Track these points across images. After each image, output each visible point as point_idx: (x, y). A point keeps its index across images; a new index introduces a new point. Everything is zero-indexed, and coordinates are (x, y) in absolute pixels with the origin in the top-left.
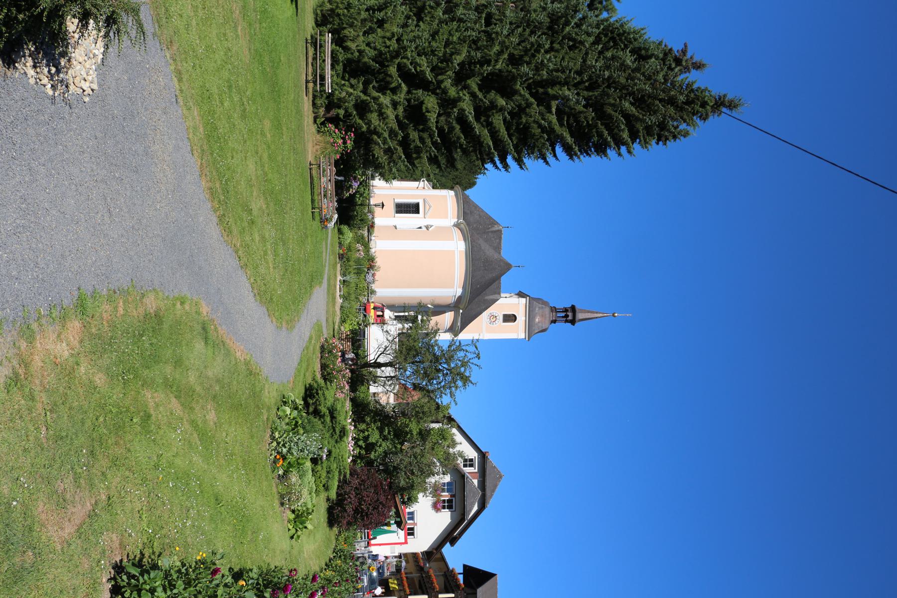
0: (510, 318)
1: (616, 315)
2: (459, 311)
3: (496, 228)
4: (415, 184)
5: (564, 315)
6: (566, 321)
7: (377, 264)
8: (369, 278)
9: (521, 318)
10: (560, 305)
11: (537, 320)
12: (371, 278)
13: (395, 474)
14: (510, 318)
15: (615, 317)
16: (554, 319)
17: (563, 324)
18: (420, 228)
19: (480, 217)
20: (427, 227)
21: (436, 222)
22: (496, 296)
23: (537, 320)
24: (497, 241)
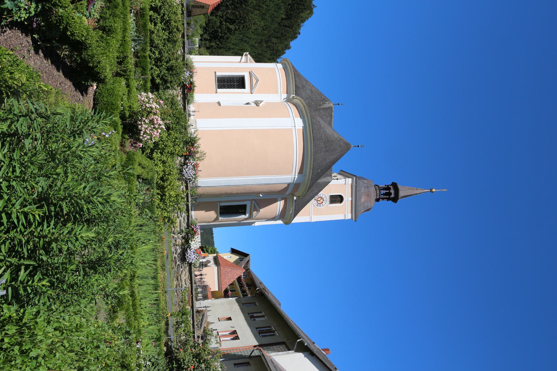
0: (337, 199)
1: (434, 190)
2: (293, 198)
3: (327, 105)
4: (239, 58)
6: (388, 199)
7: (199, 150)
9: (348, 199)
11: (363, 200)
12: (192, 172)
14: (337, 199)
15: (433, 192)
16: (378, 197)
18: (248, 104)
19: (312, 92)
20: (257, 103)
21: (266, 98)
22: (328, 178)
23: (363, 200)
24: (329, 119)
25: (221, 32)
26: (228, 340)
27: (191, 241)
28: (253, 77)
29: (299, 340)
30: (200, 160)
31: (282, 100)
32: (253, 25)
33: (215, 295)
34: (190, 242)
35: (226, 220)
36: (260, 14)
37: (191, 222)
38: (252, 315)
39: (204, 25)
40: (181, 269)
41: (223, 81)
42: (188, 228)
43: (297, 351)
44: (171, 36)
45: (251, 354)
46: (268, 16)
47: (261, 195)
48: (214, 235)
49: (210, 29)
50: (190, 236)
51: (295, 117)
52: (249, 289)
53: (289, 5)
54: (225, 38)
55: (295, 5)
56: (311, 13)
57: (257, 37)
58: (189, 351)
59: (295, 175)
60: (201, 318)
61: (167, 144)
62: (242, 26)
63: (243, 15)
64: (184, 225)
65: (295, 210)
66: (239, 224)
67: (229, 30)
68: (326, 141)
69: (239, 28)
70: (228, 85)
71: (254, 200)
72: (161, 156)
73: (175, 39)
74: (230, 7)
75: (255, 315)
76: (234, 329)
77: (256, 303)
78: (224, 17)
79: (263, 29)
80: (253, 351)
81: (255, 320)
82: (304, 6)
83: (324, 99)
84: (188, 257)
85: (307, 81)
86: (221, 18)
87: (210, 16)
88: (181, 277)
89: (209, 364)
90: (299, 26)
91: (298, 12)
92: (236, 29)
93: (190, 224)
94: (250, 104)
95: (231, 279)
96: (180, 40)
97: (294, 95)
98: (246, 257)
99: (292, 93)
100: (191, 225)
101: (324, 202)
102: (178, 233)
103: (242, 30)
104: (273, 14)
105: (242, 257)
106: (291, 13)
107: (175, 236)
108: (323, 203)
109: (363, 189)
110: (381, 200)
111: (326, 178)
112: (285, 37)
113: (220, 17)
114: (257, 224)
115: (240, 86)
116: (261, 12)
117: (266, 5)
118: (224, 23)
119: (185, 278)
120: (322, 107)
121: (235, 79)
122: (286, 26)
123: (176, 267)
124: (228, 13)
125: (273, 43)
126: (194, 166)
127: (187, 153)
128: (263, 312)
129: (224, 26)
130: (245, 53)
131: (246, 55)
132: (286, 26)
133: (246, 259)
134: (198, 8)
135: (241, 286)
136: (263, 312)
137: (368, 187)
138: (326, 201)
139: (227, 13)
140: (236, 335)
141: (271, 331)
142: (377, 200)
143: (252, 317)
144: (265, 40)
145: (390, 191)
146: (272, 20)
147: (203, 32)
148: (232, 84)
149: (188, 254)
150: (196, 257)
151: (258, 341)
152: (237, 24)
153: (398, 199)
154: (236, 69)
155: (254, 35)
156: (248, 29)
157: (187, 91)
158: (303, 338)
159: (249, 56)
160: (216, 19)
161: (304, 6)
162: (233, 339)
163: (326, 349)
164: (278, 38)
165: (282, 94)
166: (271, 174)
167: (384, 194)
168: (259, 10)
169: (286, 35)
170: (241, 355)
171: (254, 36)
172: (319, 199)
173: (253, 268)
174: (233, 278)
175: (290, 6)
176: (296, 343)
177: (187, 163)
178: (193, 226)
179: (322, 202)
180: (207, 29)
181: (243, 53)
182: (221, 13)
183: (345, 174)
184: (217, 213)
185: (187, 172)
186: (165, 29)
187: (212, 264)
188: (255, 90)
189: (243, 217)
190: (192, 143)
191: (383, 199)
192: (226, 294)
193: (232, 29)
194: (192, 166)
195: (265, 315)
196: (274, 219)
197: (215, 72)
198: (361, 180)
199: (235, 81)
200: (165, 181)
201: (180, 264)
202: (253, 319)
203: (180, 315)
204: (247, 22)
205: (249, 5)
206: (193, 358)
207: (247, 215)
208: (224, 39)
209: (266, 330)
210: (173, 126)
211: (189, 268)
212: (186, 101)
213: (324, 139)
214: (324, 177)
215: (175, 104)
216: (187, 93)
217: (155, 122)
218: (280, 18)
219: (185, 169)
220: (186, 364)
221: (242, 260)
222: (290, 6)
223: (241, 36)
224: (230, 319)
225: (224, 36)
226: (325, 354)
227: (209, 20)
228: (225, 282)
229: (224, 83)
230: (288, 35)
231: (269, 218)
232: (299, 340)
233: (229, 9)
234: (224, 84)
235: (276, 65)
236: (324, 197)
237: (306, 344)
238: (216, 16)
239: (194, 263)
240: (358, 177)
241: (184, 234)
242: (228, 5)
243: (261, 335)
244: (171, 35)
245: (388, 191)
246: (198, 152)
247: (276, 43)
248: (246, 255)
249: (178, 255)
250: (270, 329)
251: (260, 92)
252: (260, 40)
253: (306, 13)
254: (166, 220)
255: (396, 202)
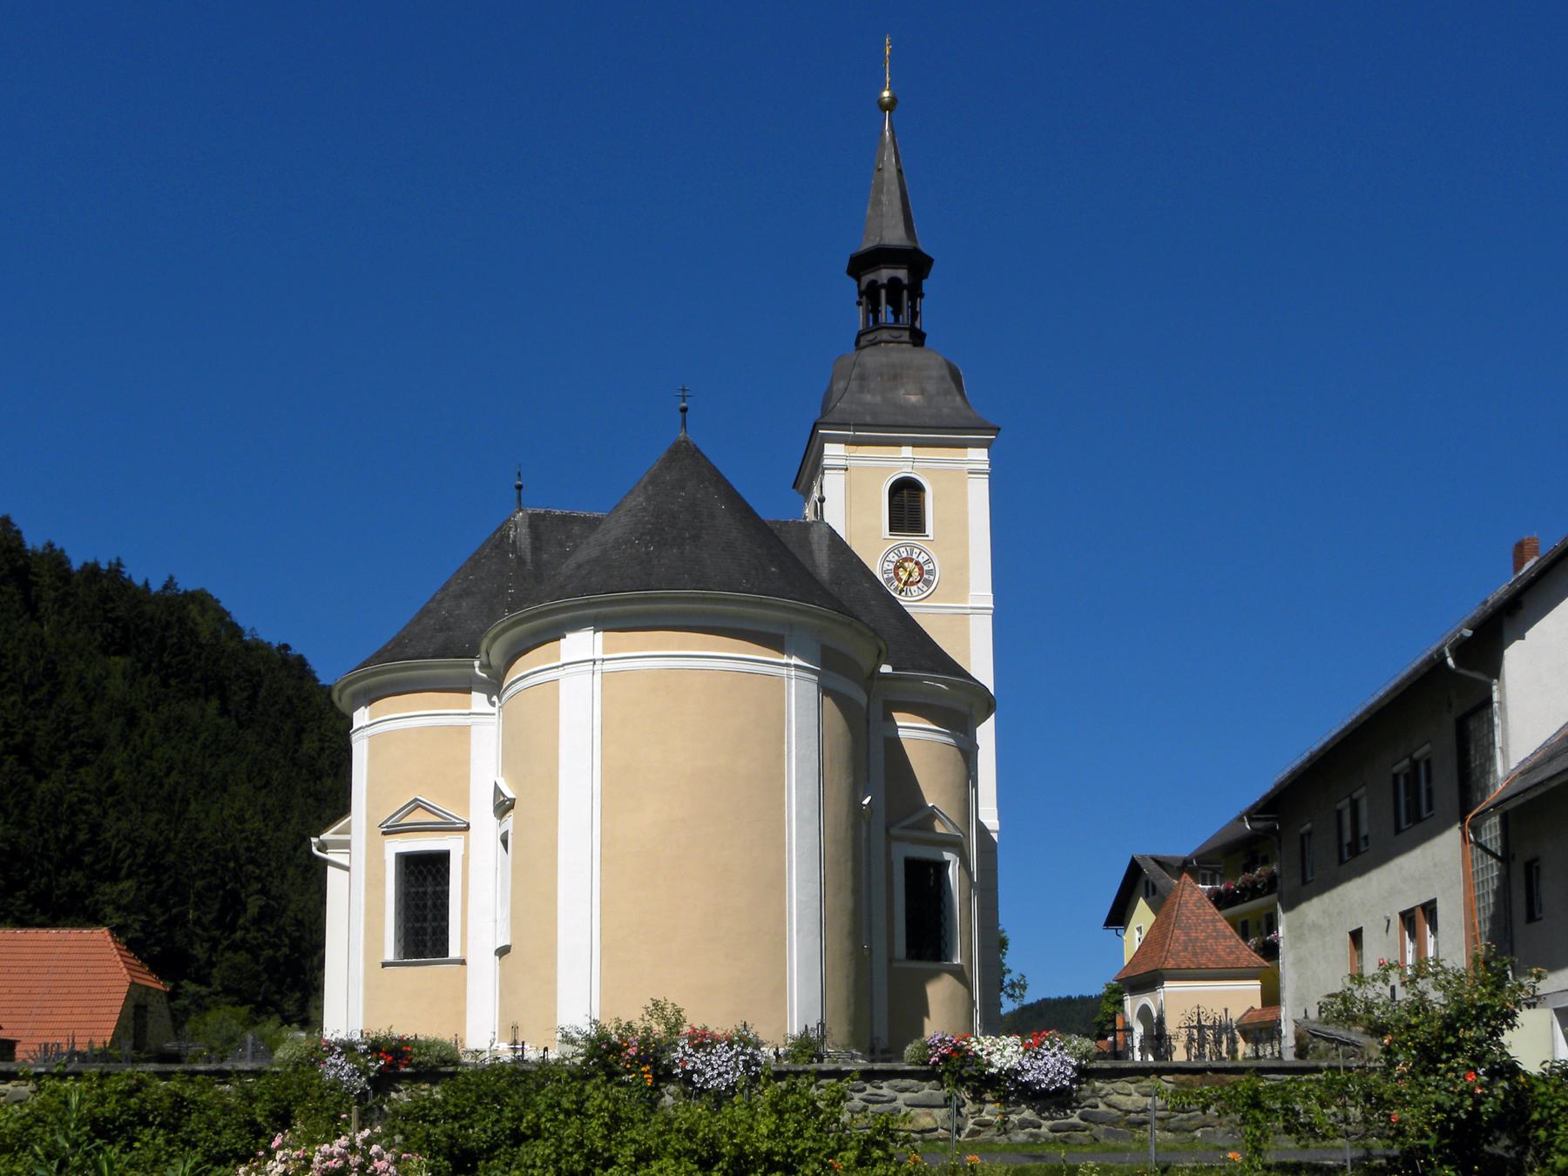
1: (886, 94)
3: (520, 533)
5: (890, 309)
6: (916, 292)
7: (638, 1025)
8: (718, 1069)
9: (905, 461)
10: (858, 317)
12: (721, 1055)
13: (567, 1062)
16: (906, 336)
17: (924, 305)
18: (505, 842)
20: (503, 807)
23: (913, 399)
25: (276, 947)
26: (1436, 944)
27: (990, 1064)
28: (404, 821)
29: (1450, 661)
30: (679, 1023)
31: (494, 710)
32: (247, 826)
33: (1271, 997)
34: (993, 1070)
35: (965, 939)
36: (205, 797)
37: (916, 1064)
38: (1346, 850)
39: (244, 1010)
40: (1102, 1108)
41: (417, 934)
42: (939, 1077)
43: (1495, 669)
44: (159, 1119)
45: (1494, 855)
46: (213, 766)
47: (866, 802)
48: (1075, 994)
49: (260, 986)
50: (969, 1069)
51: (559, 659)
52: (1265, 861)
53: (165, 683)
54: (297, 934)
55: (166, 660)
56: (201, 599)
57: (297, 813)
58: (1403, 1086)
59: (787, 665)
60: (1322, 1045)
61: (571, 1141)
62: (250, 868)
63: (207, 862)
64: (926, 1091)
65: (932, 671)
66: (986, 888)
67: (263, 917)
68: (657, 538)
69: (258, 879)
70: (435, 919)
71: (887, 830)
72: (620, 1166)
73: (167, 1102)
74: (174, 911)
75: (1347, 837)
76: (1396, 921)
77: (1302, 830)
78: (217, 933)
79: (267, 784)
80: (1480, 846)
81: (1366, 838)
82: (168, 623)
83: (497, 547)
84: (1052, 1081)
85: (425, 612)
86: (221, 947)
87: (209, 985)
88: (1130, 1112)
89: (1466, 1010)
90: (256, 648)
91: (194, 650)
92: (263, 892)
93: (924, 1068)
94: (507, 832)
95: (1215, 930)
96: (173, 1085)
97: (477, 663)
98: (1141, 870)
99: (469, 670)
100: (926, 1063)
101: (914, 556)
102: (959, 1113)
103: (267, 869)
104: (205, 747)
105: (1141, 887)
106: (198, 675)
107: (970, 1125)
108: (921, 561)
109: (868, 398)
110: (918, 325)
111: (815, 547)
112: (295, 701)
113: (213, 949)
114: (989, 815)
115: (438, 871)
116: (196, 793)
117: (168, 774)
118: (239, 934)
119: (1136, 1096)
120: (528, 556)
121: (413, 890)
122: (252, 698)
123: (1092, 1125)
124: (199, 918)
125: (322, 749)
126: (696, 1048)
127: (648, 1073)
128: (1339, 806)
129: (249, 936)
130: (314, 850)
131: (323, 847)
132: (252, 698)
133: (1149, 869)
134: (145, 1026)
135: (1251, 892)
136: (1339, 806)
137: (862, 378)
138: (913, 547)
139: (198, 922)
140: (1419, 913)
141: (1412, 777)
142: (918, 338)
143: (1355, 849)
144: (307, 781)
145: (883, 286)
146: (230, 750)
147: (272, 1014)
148: (430, 903)
149: (1040, 1082)
150: (1055, 1049)
151: (1447, 826)
152: (243, 886)
153: (916, 251)
154: (374, 884)
155: (288, 821)
156: (264, 844)
157: (406, 1066)
158: (1443, 646)
159: (326, 836)
160: (225, 965)
161: (168, 623)
162: (1434, 929)
163: (1515, 556)
164: (302, 730)
165: (473, 710)
166: (780, 756)
167: (897, 313)
168: (185, 802)
169: (289, 700)
170: (1496, 893)
171: (294, 821)
172: (904, 577)
173: (1184, 847)
174: (1214, 921)
175: (173, 682)
176: (1462, 671)
177: (685, 1072)
178: (931, 1056)
179: (917, 563)
180: (260, 998)
181: (317, 858)
182: (197, 946)
183: (809, 470)
184: (935, 975)
185: (720, 1075)
186: (128, 1138)
187: (1154, 1001)
188: (455, 812)
189: (953, 873)
190: (608, 1052)
191: (914, 315)
192: (1270, 951)
193: (261, 907)
194: (697, 1052)
195: (1350, 795)
196: (968, 754)
197: (384, 965)
198: (832, 404)
199: (421, 890)
200: (714, 1152)
201: (1079, 1111)
202: (1362, 843)
203: (1260, 1116)
204: (234, 846)
205: (167, 839)
206: (1436, 1071)
207: (948, 856)
208: (301, 938)
209: (1407, 794)
210: (508, 1119)
211: (1097, 1079)
212: (442, 1069)
213: (647, 547)
214: (811, 552)
215: (424, 1108)
216: (413, 1066)
217: (337, 1166)
218: (221, 721)
219: (706, 1081)
220: (1457, 1099)
221: (1154, 887)
222: (173, 682)
223: (291, 871)
224: (1356, 937)
225: (289, 936)
226: (1535, 559)
227: (227, 991)
228: (1229, 954)
229: (425, 934)
230: (290, 692)
231: (964, 772)
232: (1450, 661)
233: (184, 914)
234: (430, 930)
235: (359, 734)
236: (893, 557)
237: (1468, 633)
238: (211, 964)
239: (1081, 1059)
240: (825, 409)
241: (965, 1095)
242: (164, 918)
243: (1425, 814)
244: (155, 1118)
245: (883, 292)
246: (648, 1030)
247: (321, 740)
248: (1134, 870)
249: (1045, 1119)
250: (1407, 776)
251: (464, 798)
252: (310, 801)
253: (199, 619)
254: (877, 1153)
255: (929, 261)
